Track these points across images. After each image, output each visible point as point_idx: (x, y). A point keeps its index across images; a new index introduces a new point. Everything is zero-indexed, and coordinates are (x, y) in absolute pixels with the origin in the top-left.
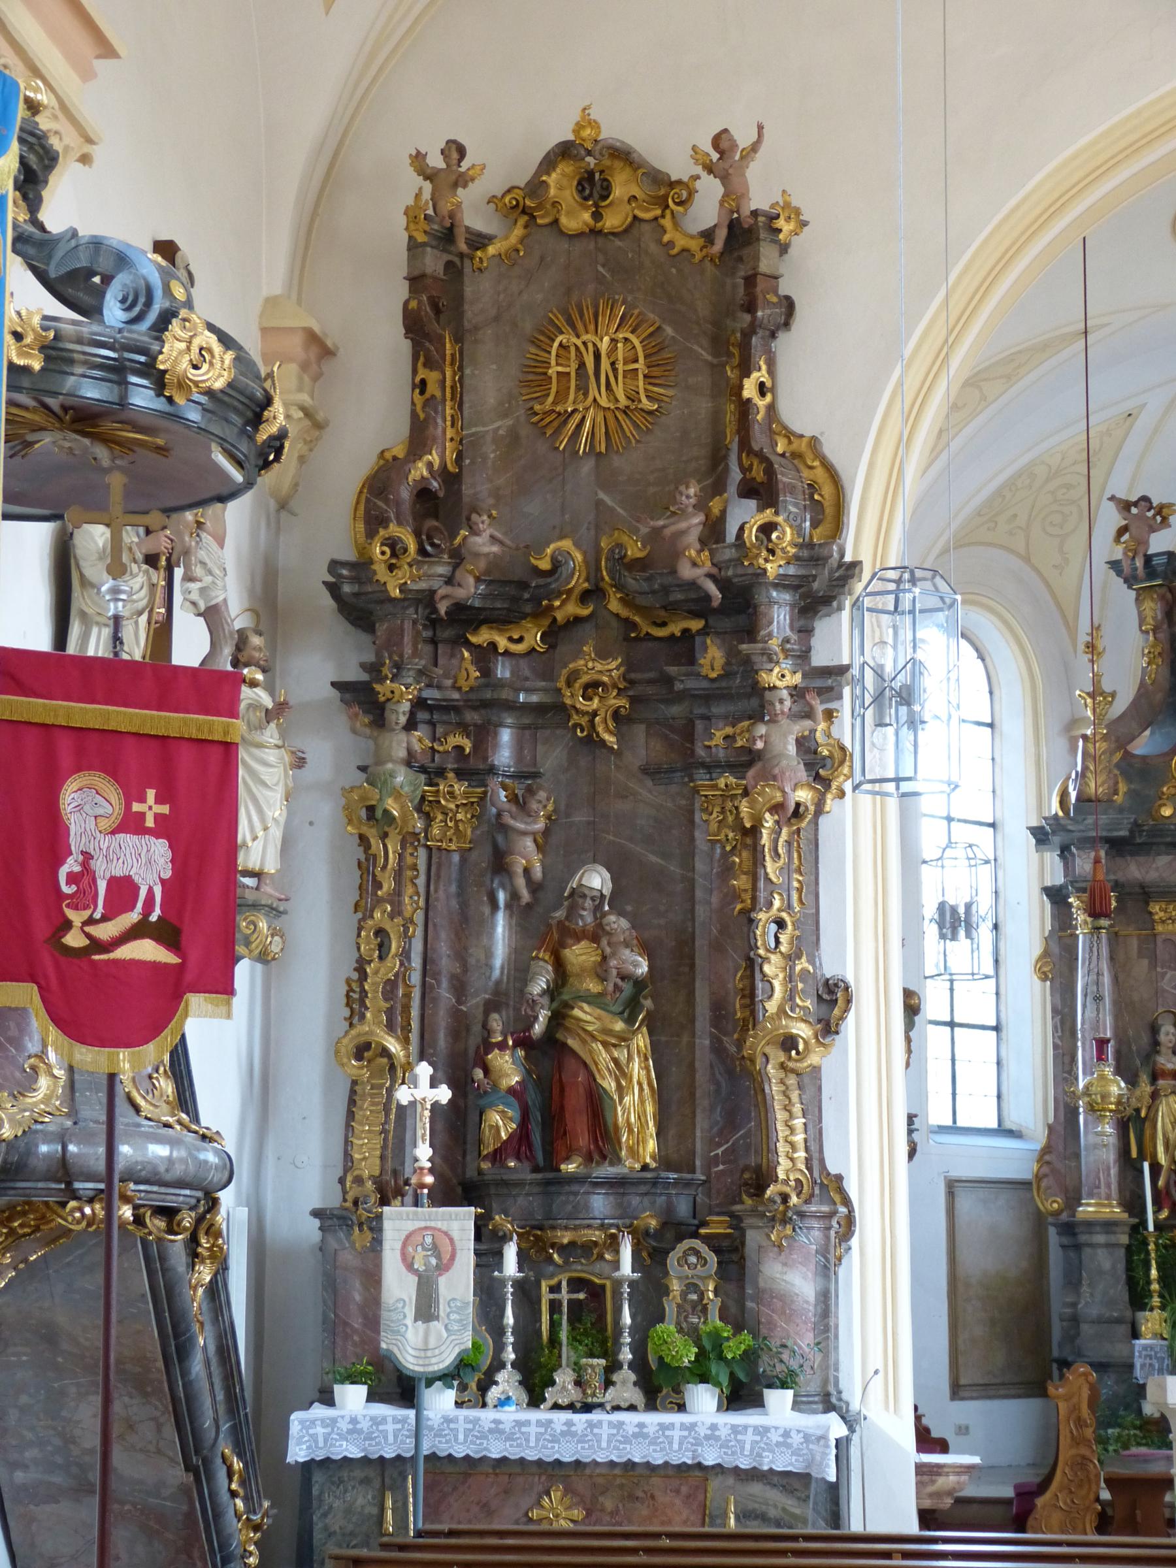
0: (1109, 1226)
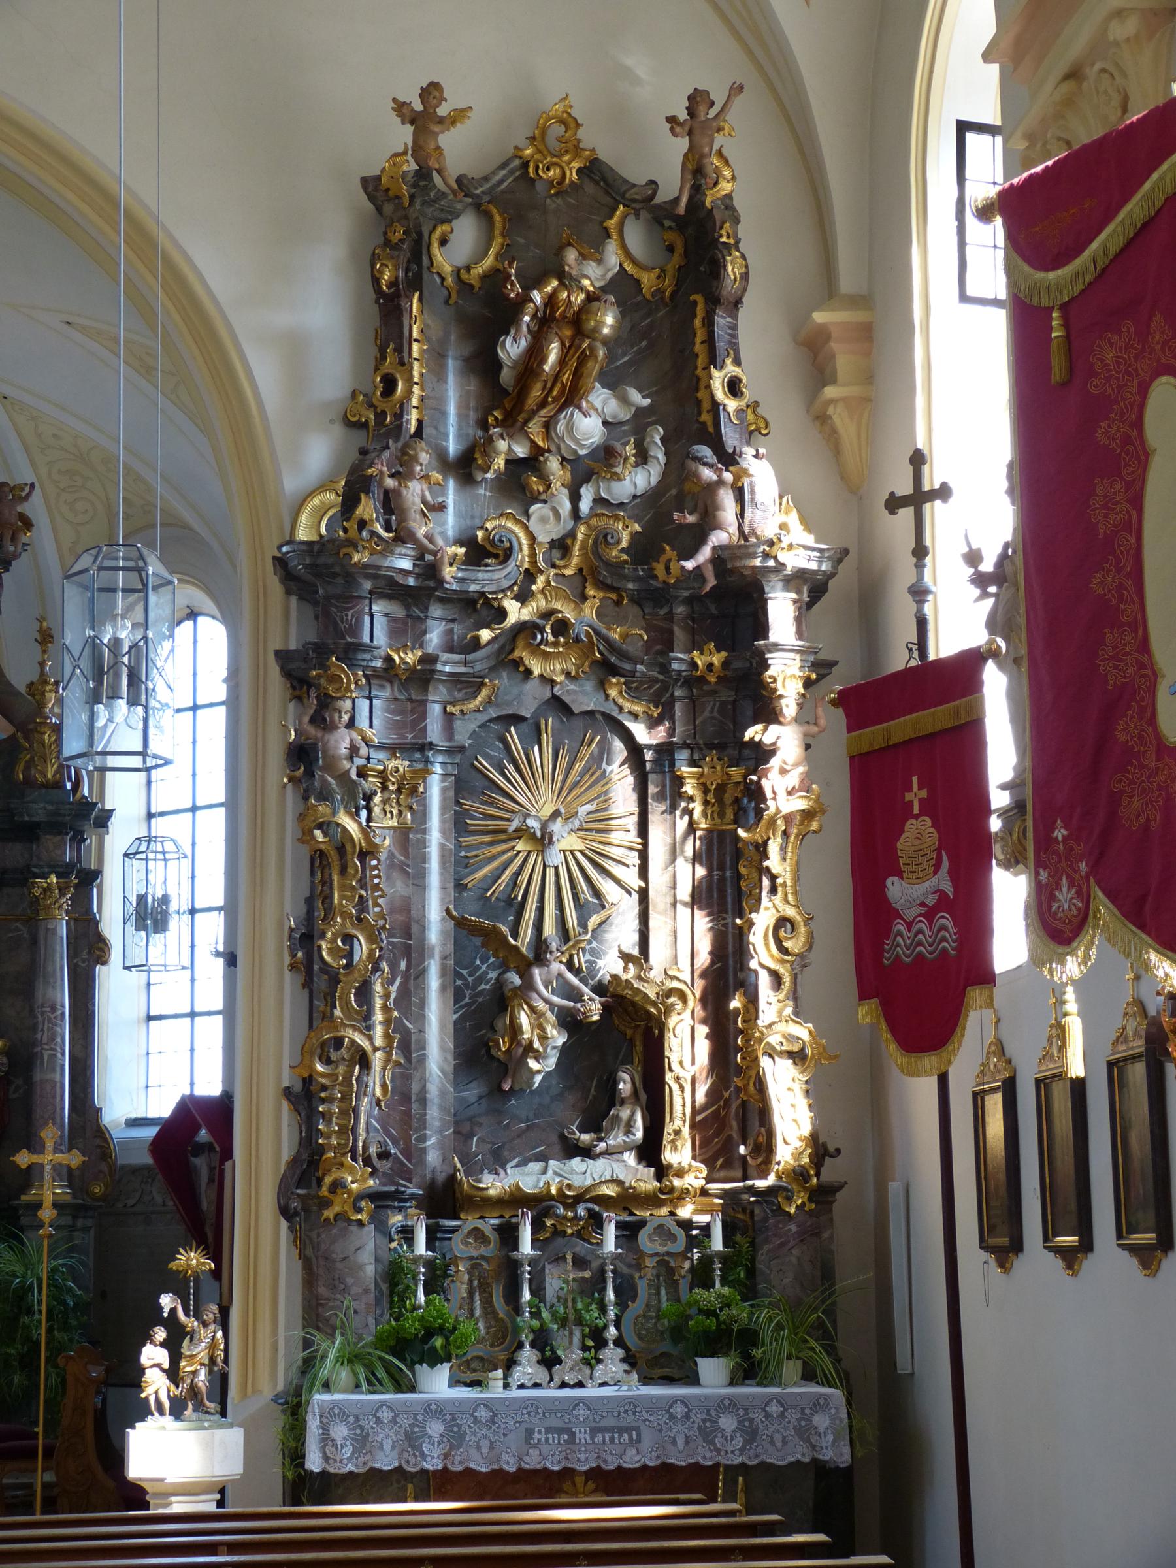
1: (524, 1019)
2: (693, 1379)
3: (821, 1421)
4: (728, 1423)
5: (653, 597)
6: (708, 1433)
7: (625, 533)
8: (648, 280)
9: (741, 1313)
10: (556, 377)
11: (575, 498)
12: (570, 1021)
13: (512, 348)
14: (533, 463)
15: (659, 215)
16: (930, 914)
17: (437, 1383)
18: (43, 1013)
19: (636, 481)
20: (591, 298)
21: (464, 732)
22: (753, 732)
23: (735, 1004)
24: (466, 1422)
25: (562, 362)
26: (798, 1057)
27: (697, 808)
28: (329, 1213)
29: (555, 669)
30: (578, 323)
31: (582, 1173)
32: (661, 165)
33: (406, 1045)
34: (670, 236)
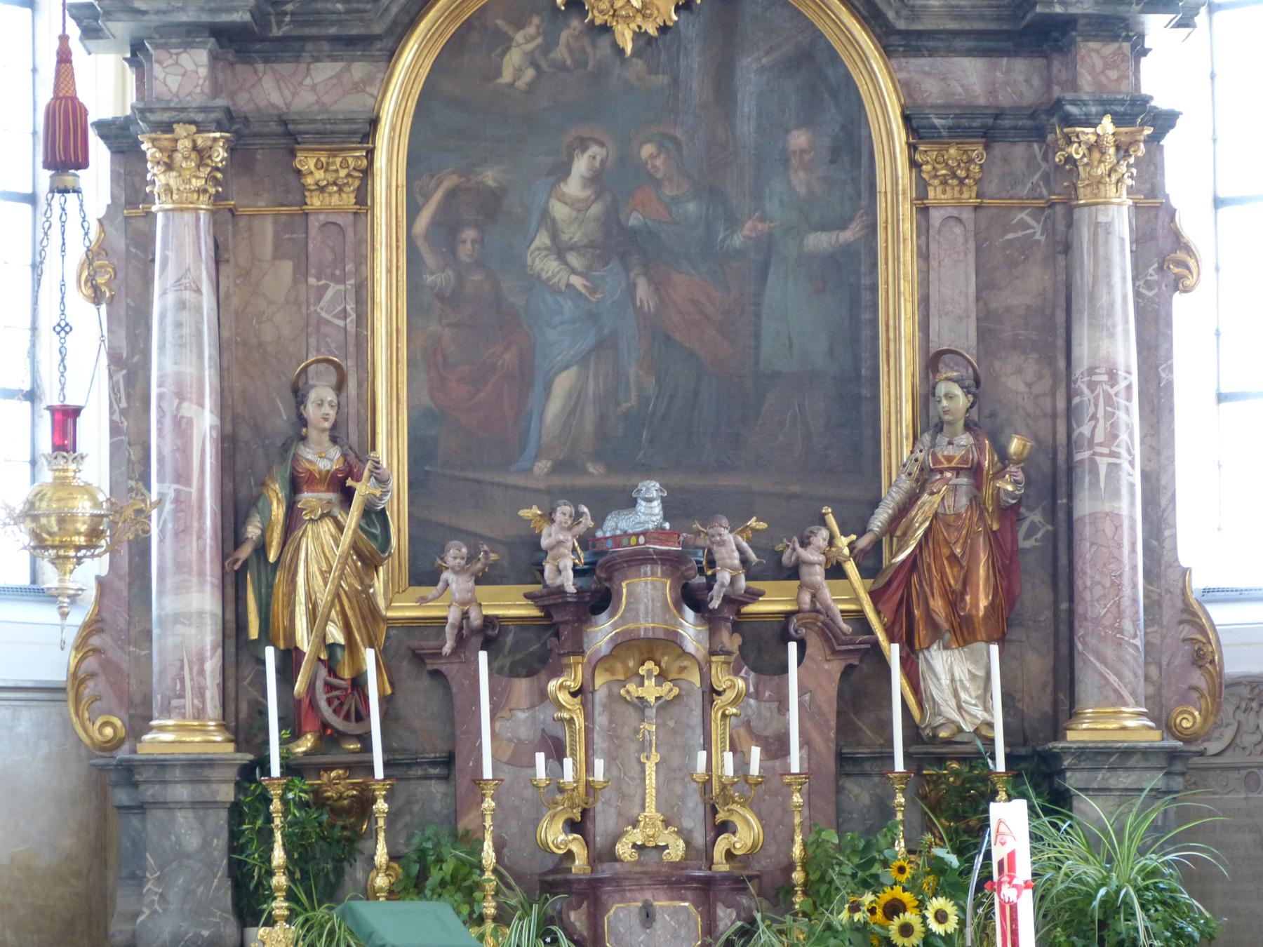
0: (198, 767)
18: (1092, 386)
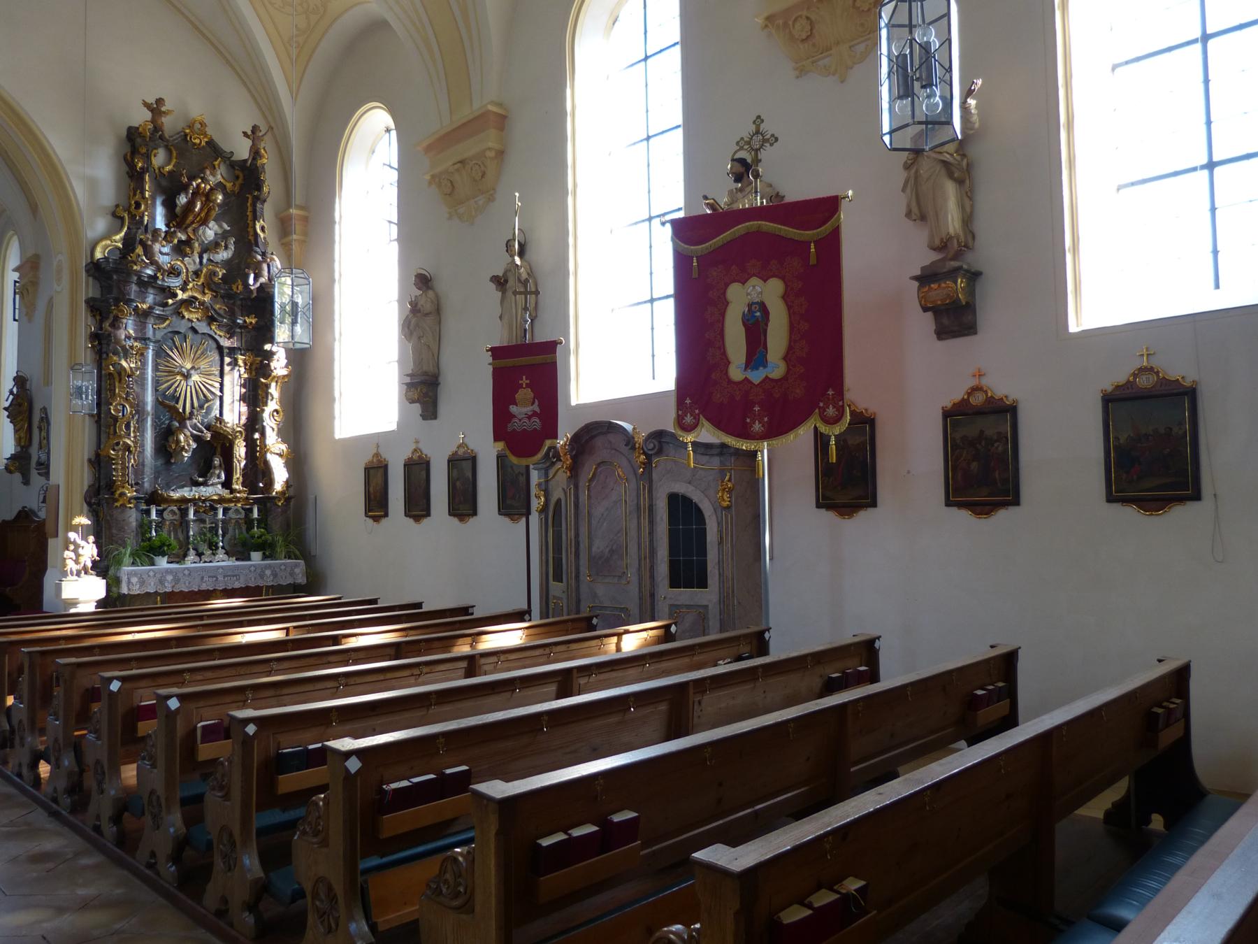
1: (182, 437)
2: (249, 559)
3: (297, 571)
4: (268, 572)
5: (229, 297)
6: (262, 576)
7: (221, 272)
8: (229, 185)
9: (269, 537)
10: (199, 214)
11: (201, 258)
12: (197, 439)
13: (183, 200)
14: (188, 242)
15: (139, 153)
16: (529, 417)
17: (163, 563)
19: (223, 255)
20: (211, 189)
21: (159, 335)
22: (267, 347)
23: (257, 436)
24: (180, 575)
25: (201, 209)
26: (280, 455)
27: (242, 370)
28: (117, 504)
29: (193, 316)
30: (208, 197)
31: (205, 492)
32: (242, 151)
33: (140, 443)
34: (237, 172)
